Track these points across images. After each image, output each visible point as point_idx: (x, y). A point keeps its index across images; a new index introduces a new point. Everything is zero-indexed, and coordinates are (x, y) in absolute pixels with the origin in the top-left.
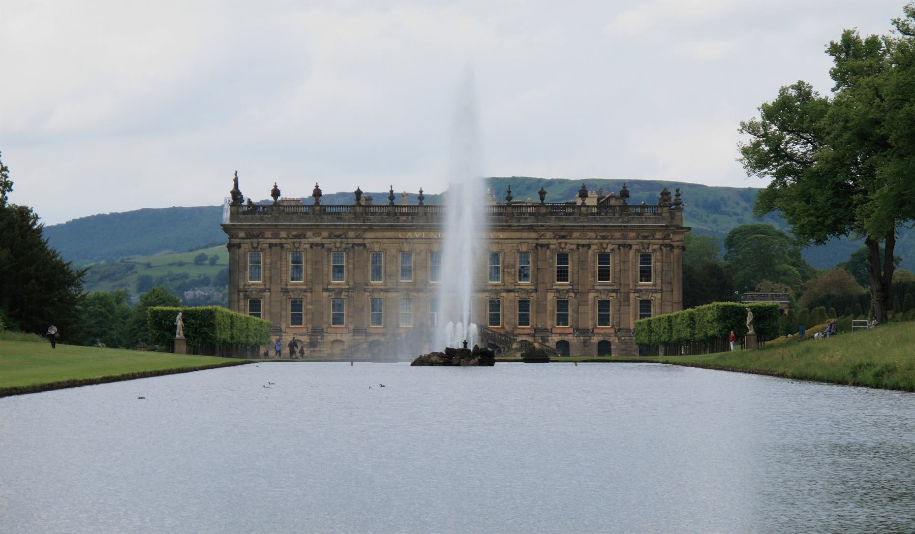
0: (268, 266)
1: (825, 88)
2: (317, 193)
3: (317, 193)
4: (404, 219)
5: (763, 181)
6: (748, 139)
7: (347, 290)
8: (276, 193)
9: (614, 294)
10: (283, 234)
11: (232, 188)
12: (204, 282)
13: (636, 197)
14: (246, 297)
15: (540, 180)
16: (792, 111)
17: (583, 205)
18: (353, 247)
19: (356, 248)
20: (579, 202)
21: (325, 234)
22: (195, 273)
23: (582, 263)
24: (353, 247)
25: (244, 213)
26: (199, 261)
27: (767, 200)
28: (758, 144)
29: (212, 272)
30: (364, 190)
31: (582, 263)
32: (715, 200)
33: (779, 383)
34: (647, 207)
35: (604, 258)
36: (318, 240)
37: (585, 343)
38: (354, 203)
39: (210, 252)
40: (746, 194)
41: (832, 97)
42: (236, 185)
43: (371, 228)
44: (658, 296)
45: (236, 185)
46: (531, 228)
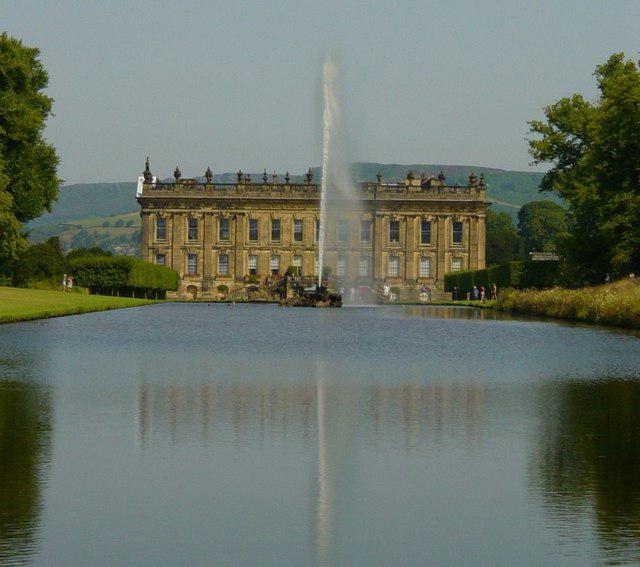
1: (593, 97)
2: (208, 175)
3: (208, 175)
4: (304, 191)
5: (547, 166)
8: (177, 174)
11: (145, 169)
12: (122, 239)
13: (452, 179)
15: (378, 165)
16: (564, 114)
17: (411, 185)
18: (172, 216)
19: (175, 216)
20: (407, 183)
22: (116, 232)
24: (172, 216)
25: (153, 189)
26: (119, 224)
27: (548, 182)
29: (130, 232)
32: (510, 181)
33: (564, 328)
34: (459, 187)
37: (411, 290)
38: (237, 182)
39: (126, 218)
40: (534, 176)
41: (596, 106)
42: (147, 168)
44: (466, 254)
45: (147, 168)
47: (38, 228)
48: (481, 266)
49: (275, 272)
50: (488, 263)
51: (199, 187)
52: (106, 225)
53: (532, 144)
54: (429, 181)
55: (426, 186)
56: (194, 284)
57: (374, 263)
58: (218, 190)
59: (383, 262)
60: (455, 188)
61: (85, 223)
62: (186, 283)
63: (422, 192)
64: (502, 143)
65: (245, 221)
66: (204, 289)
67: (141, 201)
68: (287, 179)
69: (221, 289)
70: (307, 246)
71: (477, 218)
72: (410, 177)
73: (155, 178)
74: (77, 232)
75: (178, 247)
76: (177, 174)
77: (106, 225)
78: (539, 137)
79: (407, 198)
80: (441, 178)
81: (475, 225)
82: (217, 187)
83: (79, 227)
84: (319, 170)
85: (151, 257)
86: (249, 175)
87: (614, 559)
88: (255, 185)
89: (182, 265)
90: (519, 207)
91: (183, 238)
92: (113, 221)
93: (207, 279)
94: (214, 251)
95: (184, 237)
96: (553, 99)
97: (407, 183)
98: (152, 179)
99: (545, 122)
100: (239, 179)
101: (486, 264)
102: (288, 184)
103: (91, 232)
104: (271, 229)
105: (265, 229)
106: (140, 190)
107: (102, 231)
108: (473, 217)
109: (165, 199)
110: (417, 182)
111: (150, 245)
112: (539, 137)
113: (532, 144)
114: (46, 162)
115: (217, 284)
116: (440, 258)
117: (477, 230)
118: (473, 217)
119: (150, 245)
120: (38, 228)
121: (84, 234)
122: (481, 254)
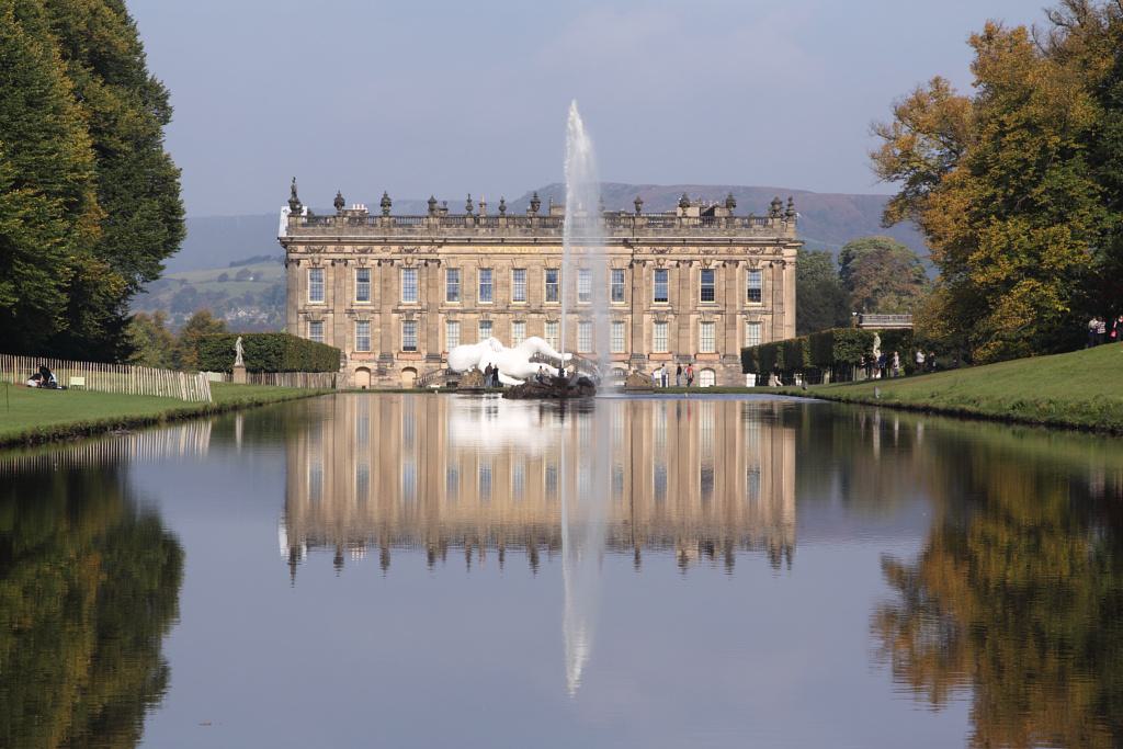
0: (331, 285)
5: (897, 187)
6: (879, 143)
7: (420, 312)
9: (719, 316)
10: (348, 248)
14: (306, 319)
16: (927, 112)
21: (395, 248)
23: (682, 281)
25: (303, 225)
28: (886, 148)
30: (440, 198)
31: (682, 281)
35: (707, 274)
36: (386, 255)
42: (294, 193)
43: (445, 243)
45: (294, 193)
46: (626, 243)
48: (788, 333)
50: (799, 328)
51: (370, 221)
52: (223, 278)
54: (712, 211)
55: (708, 216)
56: (366, 365)
57: (635, 332)
58: (400, 226)
59: (645, 332)
60: (750, 218)
62: (353, 364)
63: (701, 225)
64: (838, 161)
65: (442, 273)
66: (381, 372)
68: (469, 208)
70: (533, 308)
71: (784, 263)
72: (684, 205)
73: (305, 209)
74: (177, 289)
80: (730, 204)
81: (733, 272)
82: (398, 221)
83: (183, 281)
84: (557, 191)
85: (302, 326)
86: (445, 203)
87: (918, 707)
88: (456, 217)
89: (348, 337)
90: (840, 248)
91: (348, 297)
92: (233, 272)
94: (395, 316)
95: (351, 296)
96: (904, 92)
97: (680, 212)
98: (300, 210)
99: (890, 119)
100: (431, 210)
101: (797, 330)
102: (503, 216)
103: (201, 290)
104: (479, 283)
106: (284, 221)
107: (217, 287)
108: (777, 262)
110: (693, 212)
111: (301, 308)
114: (163, 184)
116: (731, 324)
118: (777, 262)
119: (301, 308)
122: (789, 318)
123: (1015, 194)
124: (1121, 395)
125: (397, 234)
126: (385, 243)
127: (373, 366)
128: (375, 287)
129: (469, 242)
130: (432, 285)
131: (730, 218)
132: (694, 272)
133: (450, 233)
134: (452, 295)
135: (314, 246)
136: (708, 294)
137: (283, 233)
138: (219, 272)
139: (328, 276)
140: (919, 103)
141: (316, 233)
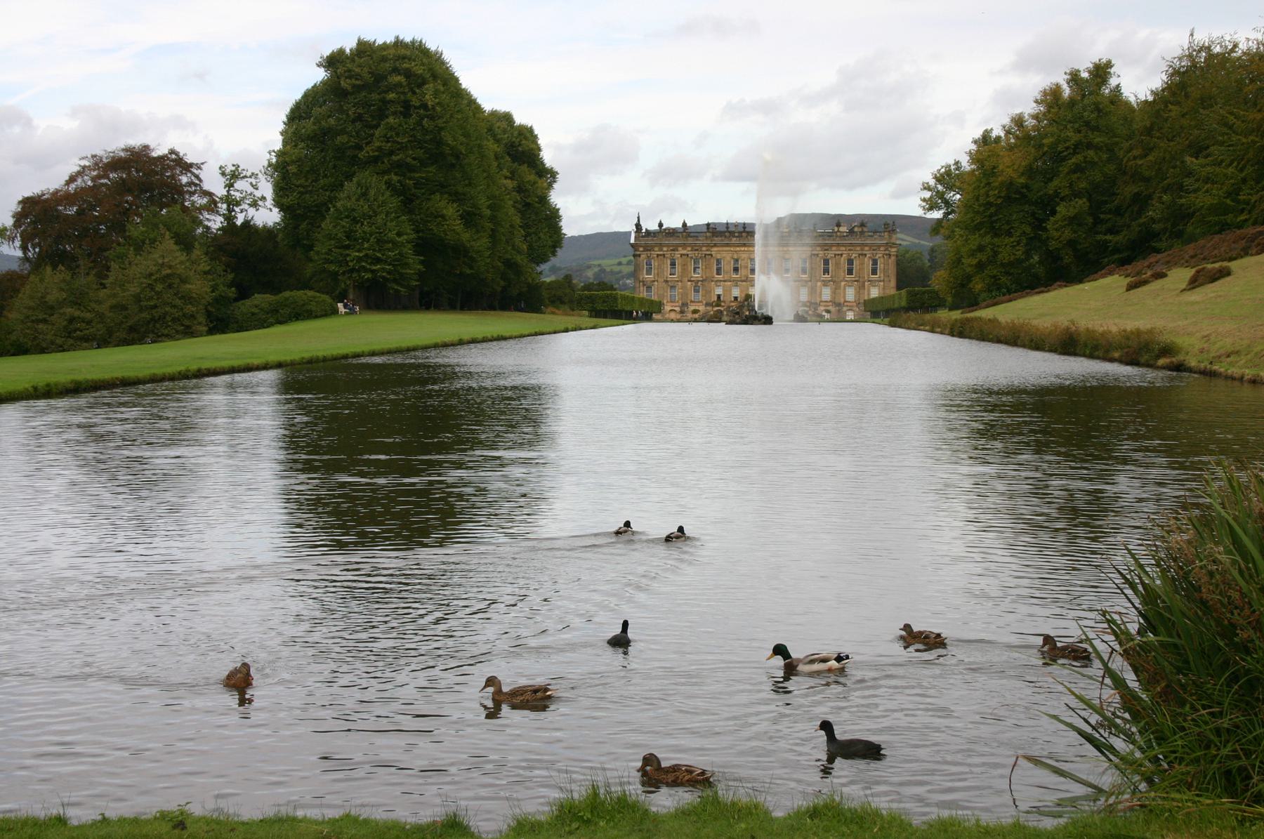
2: (684, 225)
3: (684, 225)
8: (661, 225)
23: (837, 264)
31: (837, 264)
35: (850, 262)
43: (715, 245)
47: (547, 273)
49: (736, 298)
52: (620, 264)
53: (924, 200)
55: (851, 232)
61: (605, 262)
62: (668, 308)
66: (682, 312)
67: (632, 245)
69: (695, 312)
72: (838, 225)
74: (596, 270)
75: (656, 280)
76: (661, 225)
77: (620, 264)
78: (927, 194)
79: (843, 239)
80: (862, 225)
93: (685, 305)
99: (932, 182)
103: (608, 269)
105: (727, 266)
107: (617, 269)
109: (654, 243)
112: (927, 194)
113: (957, 163)
114: (553, 217)
115: (692, 308)
117: (888, 267)
120: (547, 273)
121: (603, 271)
123: (834, 293)
124: (1261, 470)
125: (690, 241)
126: (684, 246)
127: (678, 309)
128: (678, 268)
129: (727, 245)
130: (707, 267)
131: (862, 233)
132: (843, 260)
133: (717, 240)
134: (718, 273)
135: (648, 248)
136: (850, 272)
137: (632, 241)
138: (617, 261)
139: (655, 263)
140: (948, 173)
141: (650, 241)
